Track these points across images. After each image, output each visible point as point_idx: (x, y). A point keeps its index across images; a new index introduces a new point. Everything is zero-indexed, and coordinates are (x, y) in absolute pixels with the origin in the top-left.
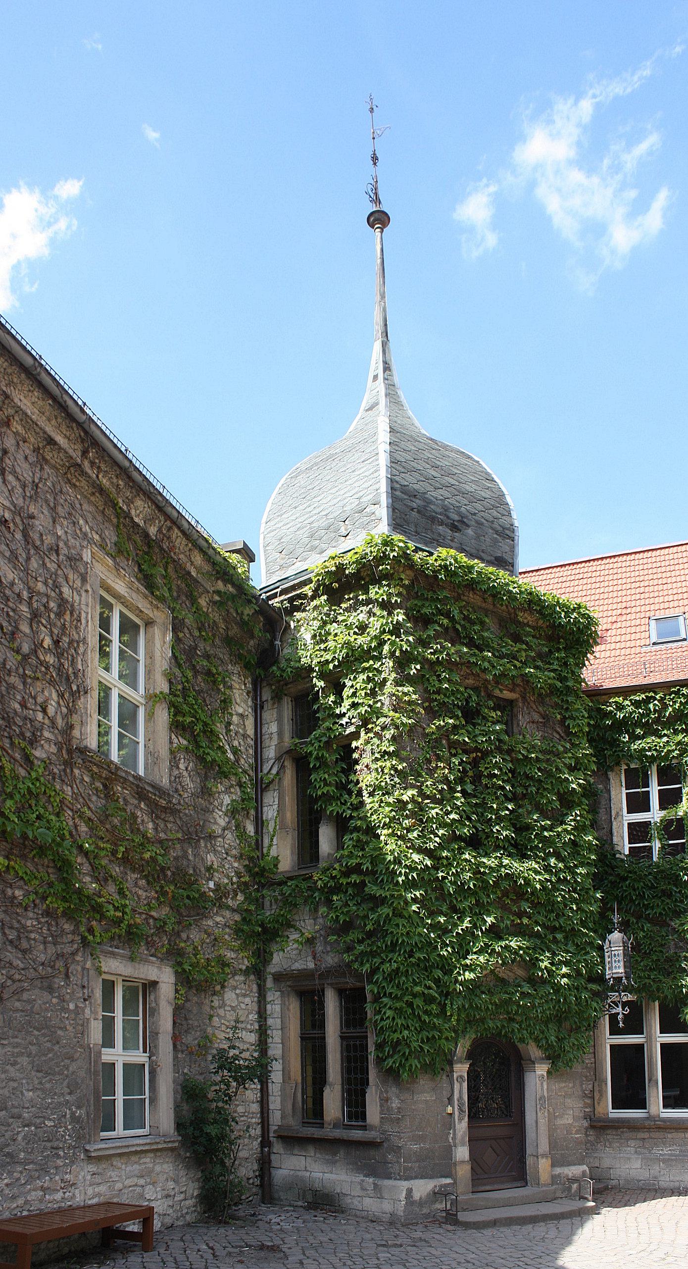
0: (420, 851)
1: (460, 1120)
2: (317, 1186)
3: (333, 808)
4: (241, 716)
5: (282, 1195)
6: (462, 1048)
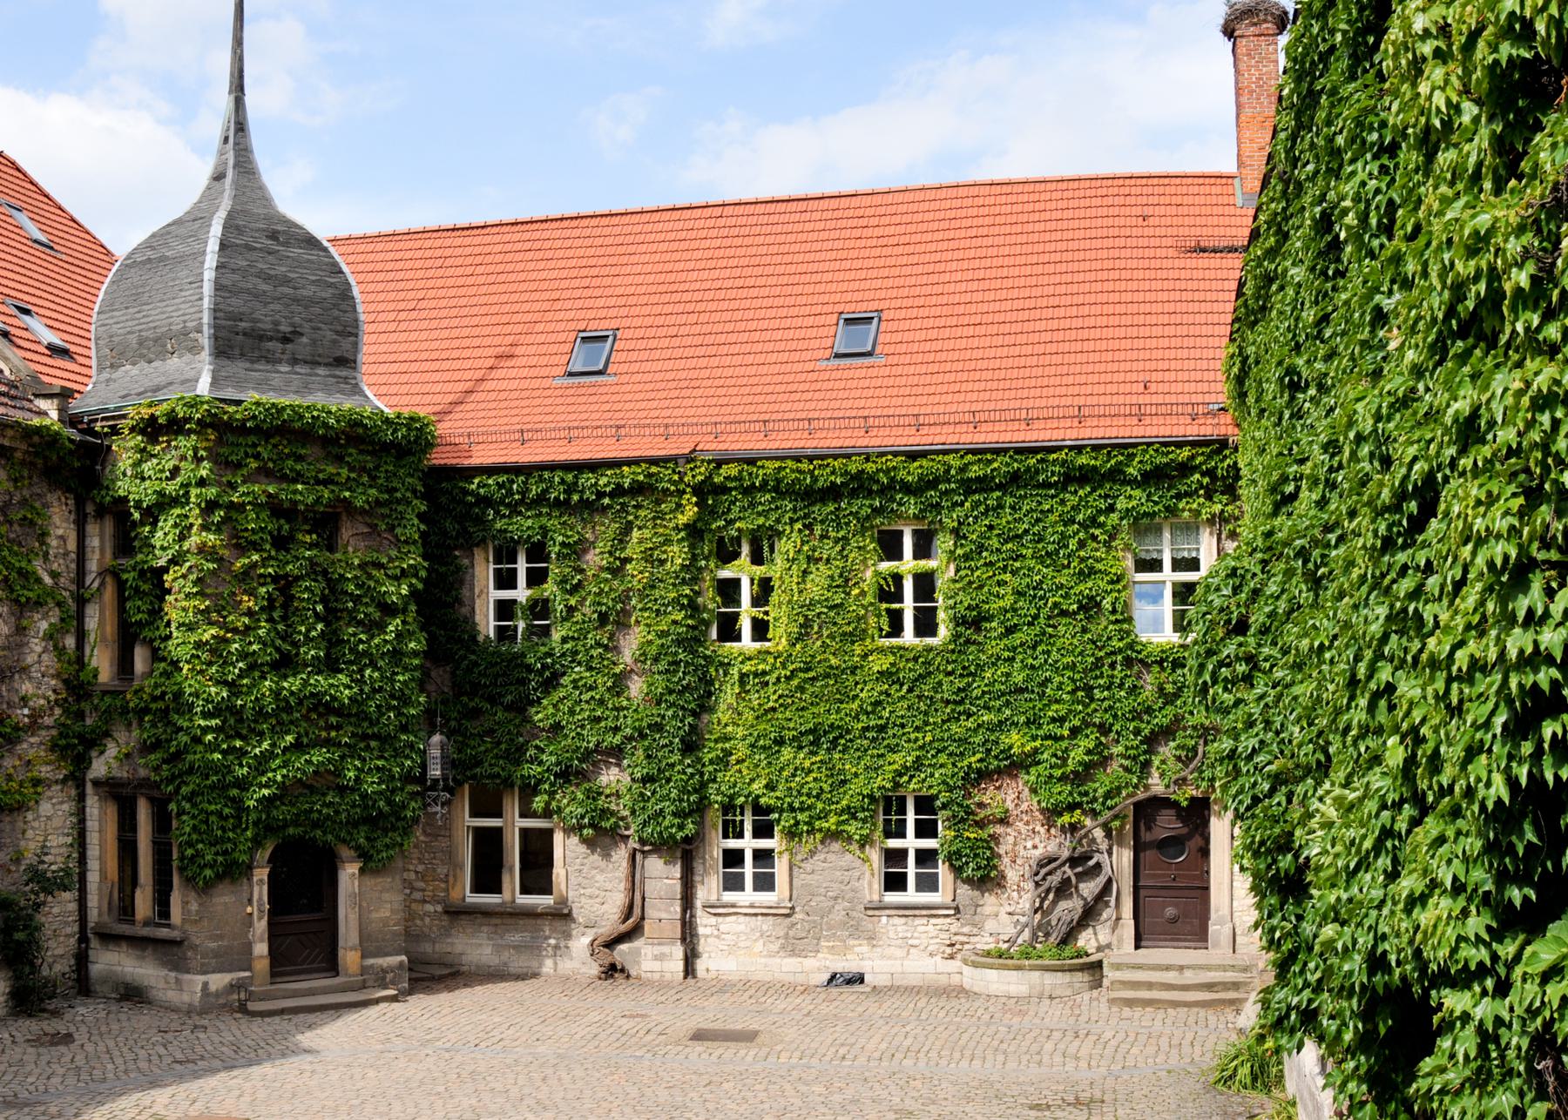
0: (218, 683)
1: (260, 919)
2: (129, 979)
3: (147, 633)
4: (62, 538)
5: (98, 988)
6: (263, 855)
